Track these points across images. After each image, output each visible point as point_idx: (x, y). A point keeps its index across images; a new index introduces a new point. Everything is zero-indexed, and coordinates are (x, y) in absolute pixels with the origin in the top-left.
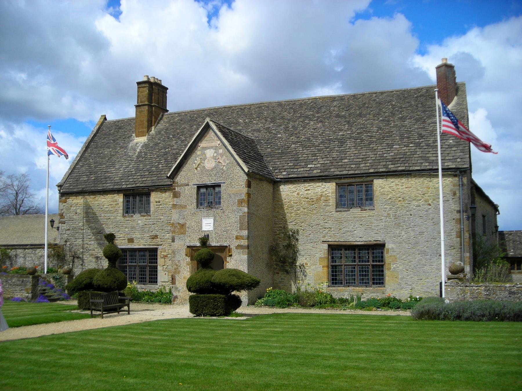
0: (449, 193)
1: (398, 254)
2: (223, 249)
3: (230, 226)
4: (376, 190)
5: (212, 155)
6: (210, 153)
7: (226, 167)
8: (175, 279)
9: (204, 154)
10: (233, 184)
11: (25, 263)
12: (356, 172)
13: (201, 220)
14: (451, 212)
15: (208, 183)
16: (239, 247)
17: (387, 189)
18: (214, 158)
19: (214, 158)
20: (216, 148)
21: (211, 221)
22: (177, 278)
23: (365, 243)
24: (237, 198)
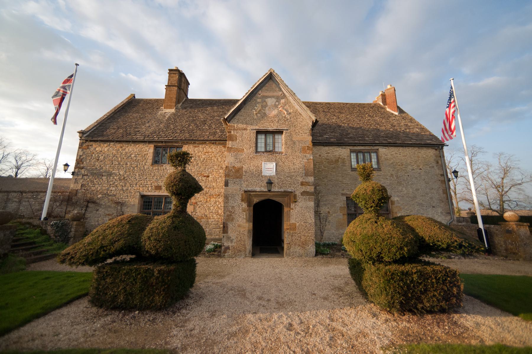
2: (287, 194)
3: (295, 172)
8: (227, 227)
9: (265, 101)
11: (19, 208)
12: (361, 142)
14: (437, 175)
16: (304, 193)
22: (230, 226)
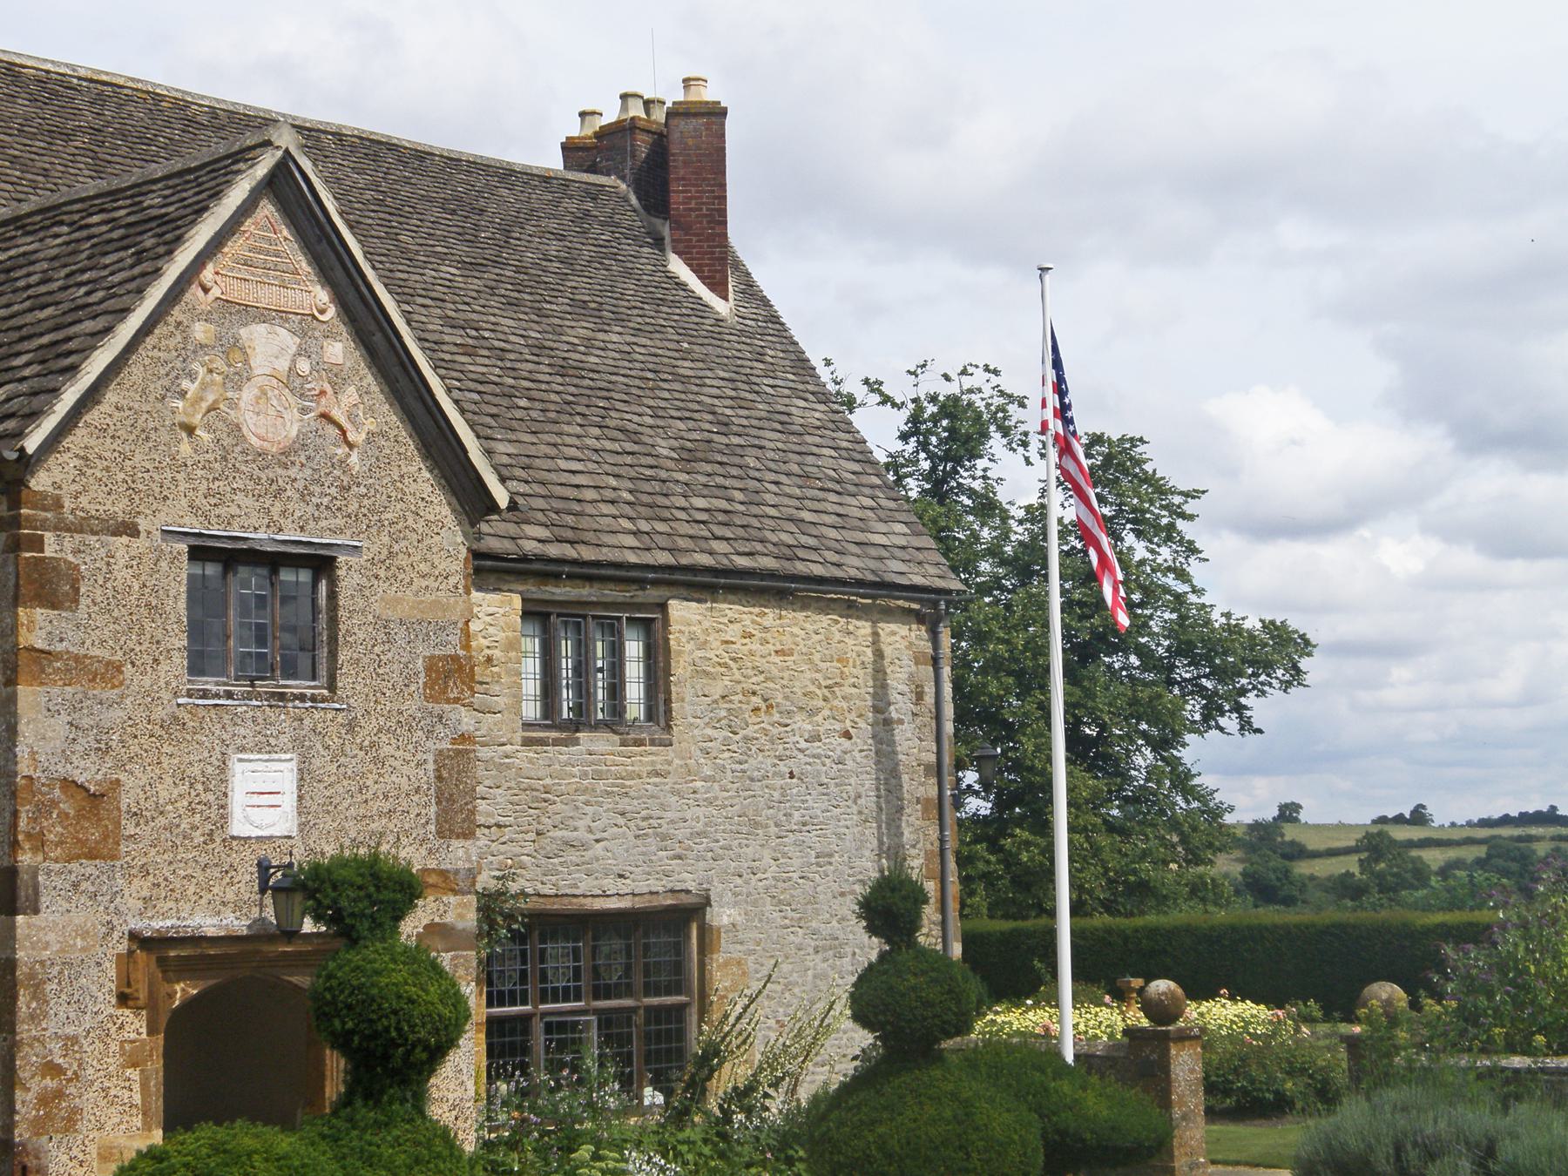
0: (906, 689)
1: (751, 952)
4: (680, 653)
5: (283, 365)
7: (364, 456)
10: (402, 561)
13: (223, 767)
15: (262, 537)
19: (291, 381)
20: (305, 325)
21: (281, 774)
23: (639, 903)
24: (424, 650)
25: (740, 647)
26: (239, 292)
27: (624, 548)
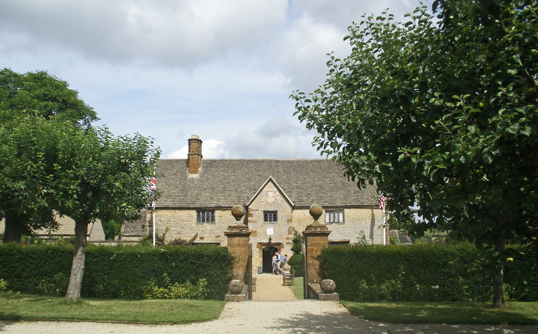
2: (279, 244)
6: (271, 194)
16: (288, 243)
17: (351, 214)
18: (273, 197)
19: (273, 197)
20: (274, 192)
21: (272, 230)
25: (355, 214)
26: (267, 190)
27: (339, 204)
